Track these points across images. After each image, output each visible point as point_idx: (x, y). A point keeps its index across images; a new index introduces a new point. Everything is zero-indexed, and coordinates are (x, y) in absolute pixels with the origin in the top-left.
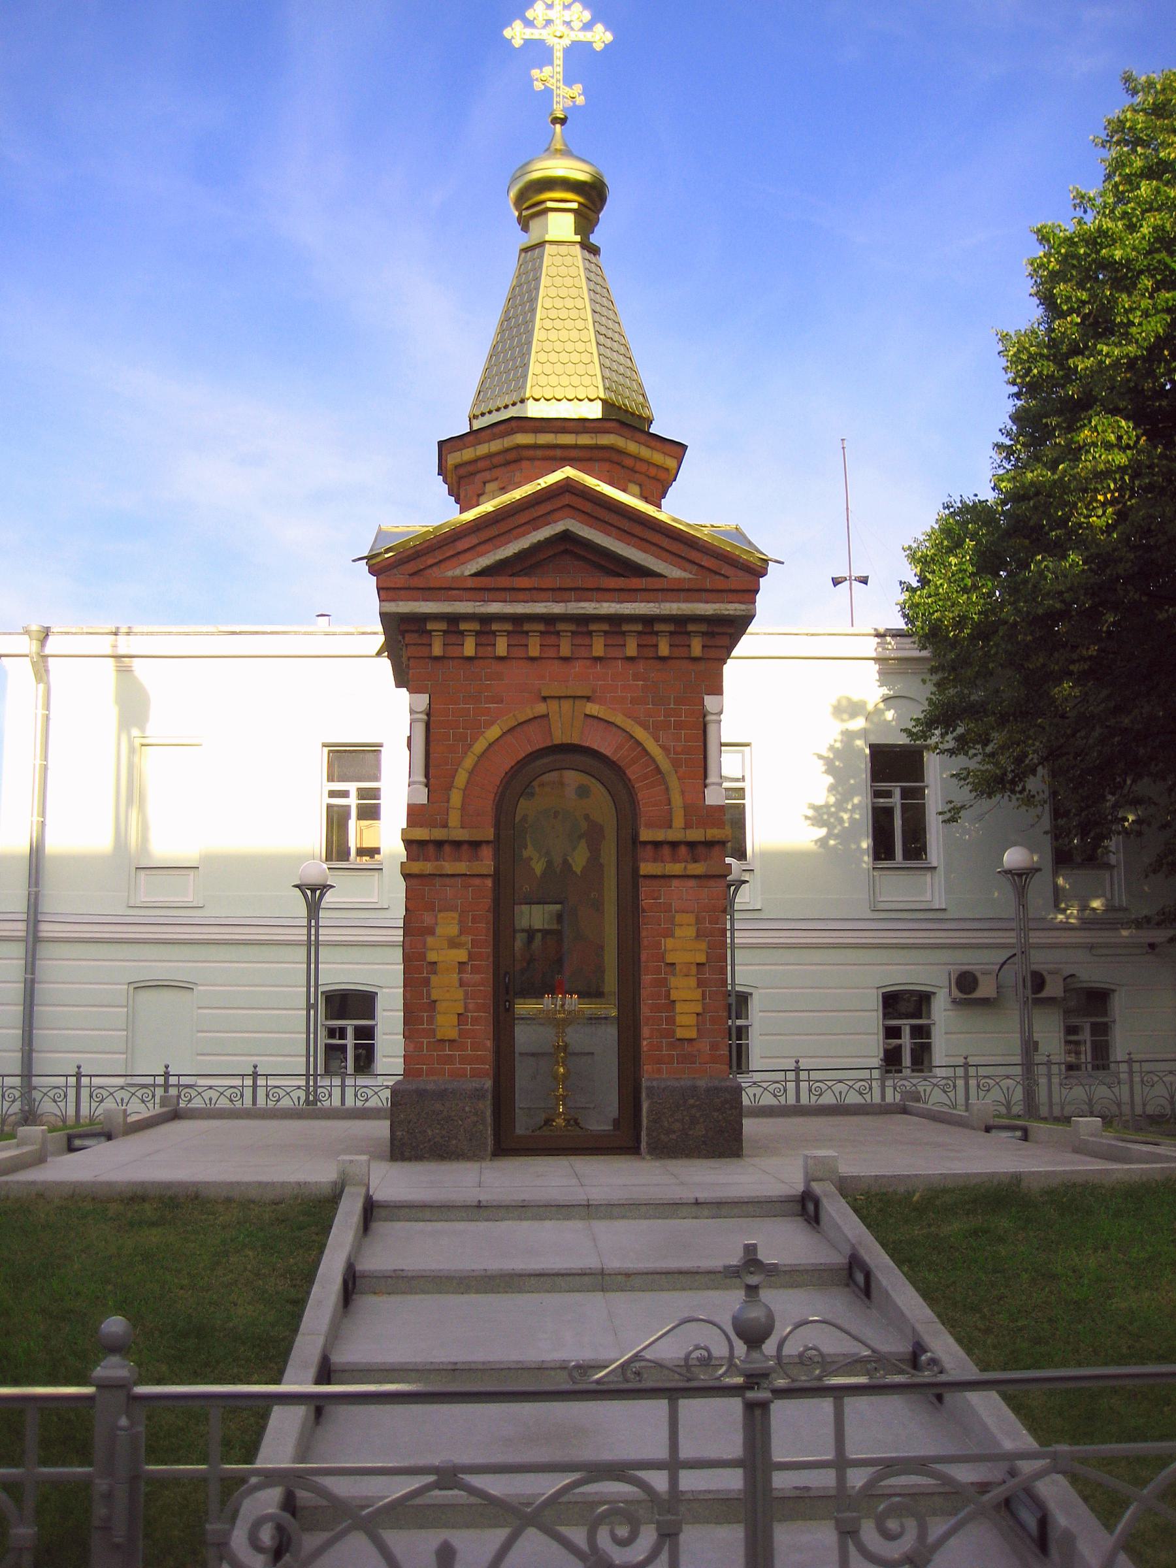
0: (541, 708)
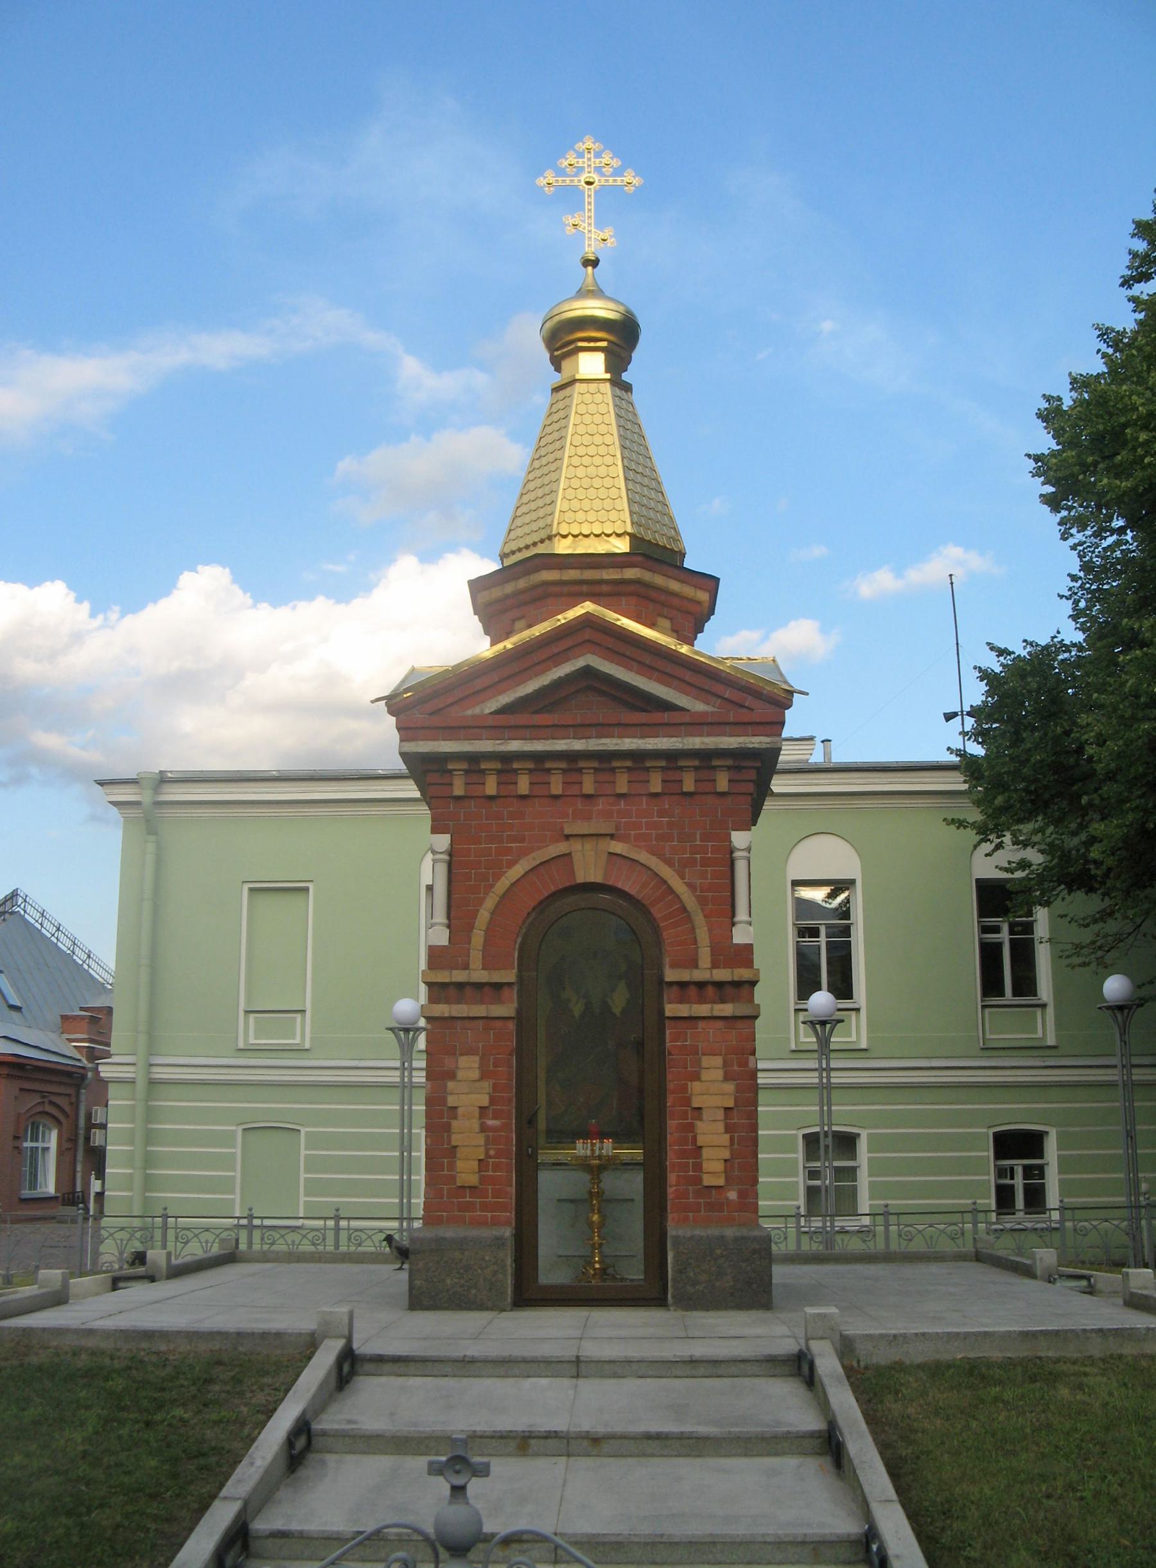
0: (561, 848)
